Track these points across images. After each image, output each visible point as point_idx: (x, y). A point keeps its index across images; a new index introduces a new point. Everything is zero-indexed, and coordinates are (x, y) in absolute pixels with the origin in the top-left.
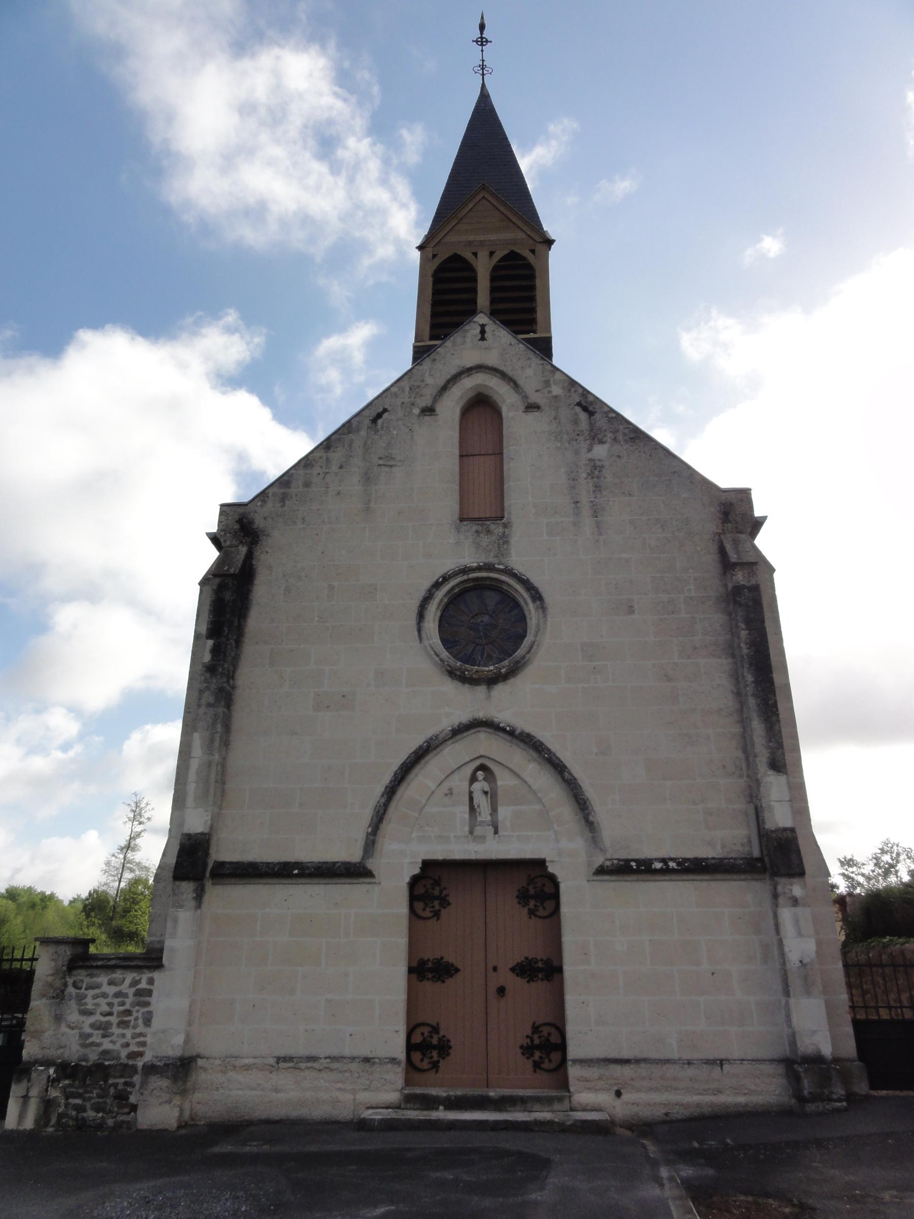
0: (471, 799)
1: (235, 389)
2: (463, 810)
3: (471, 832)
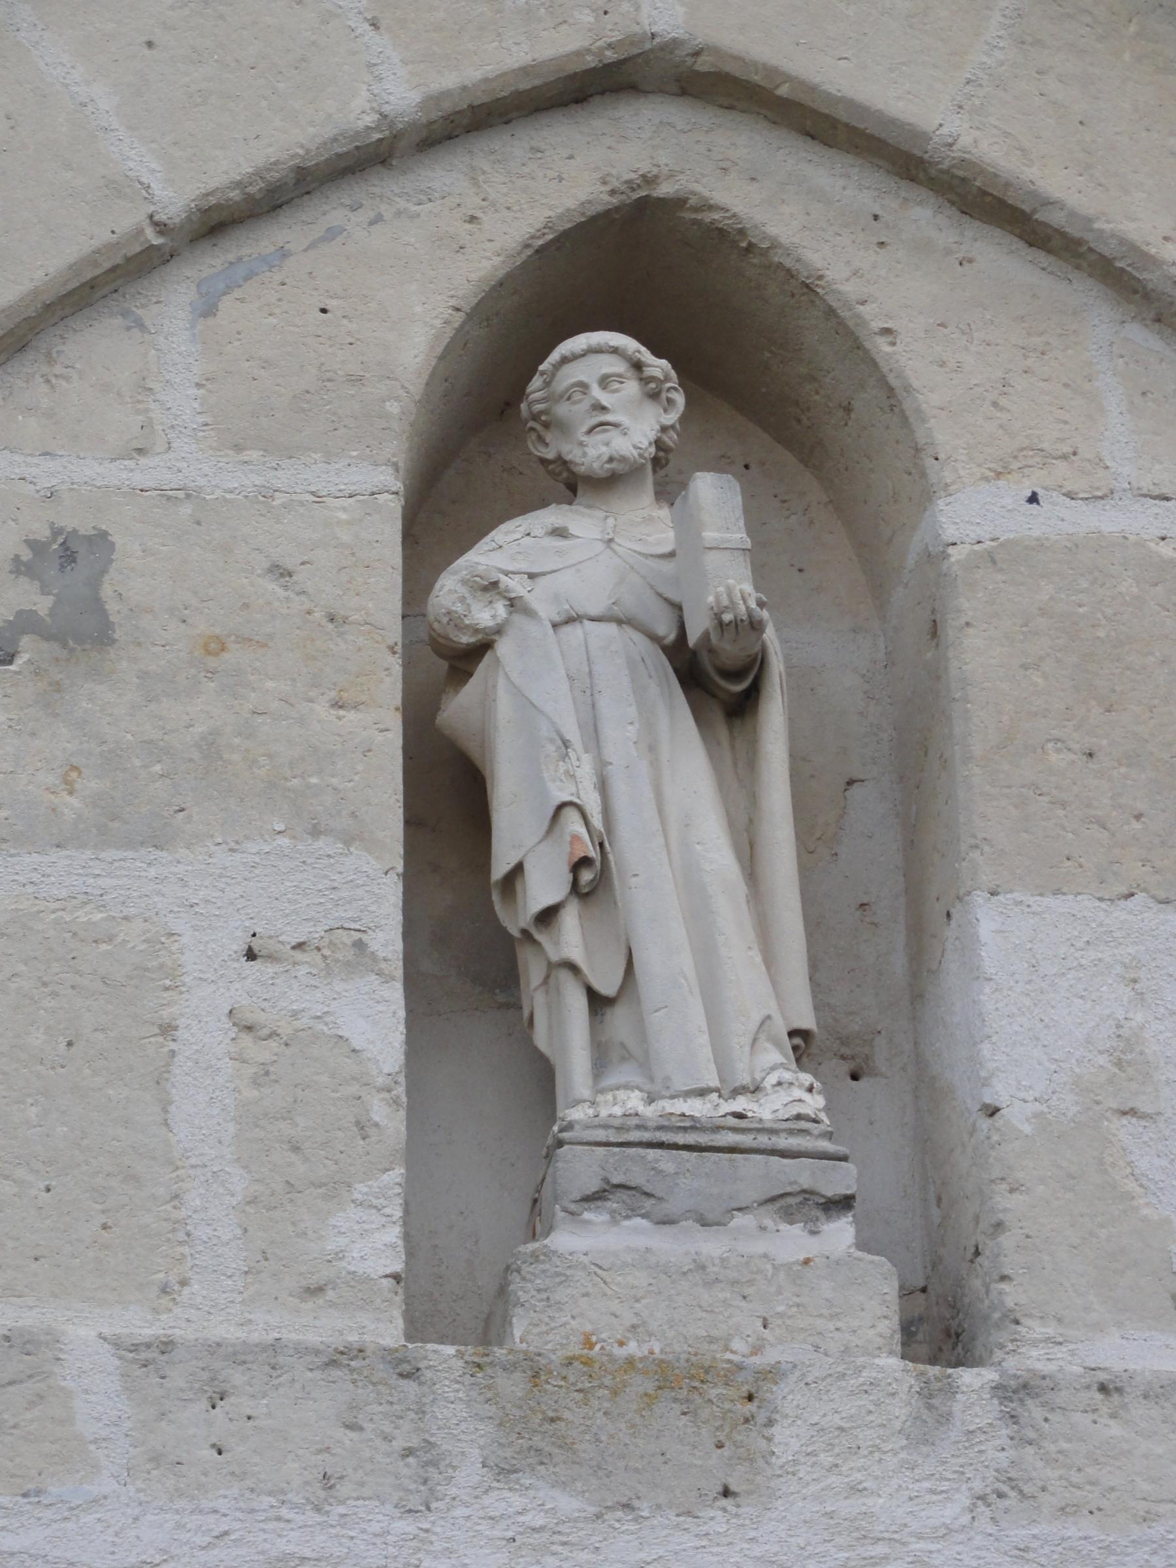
0: (448, 795)
1: (892, 397)
2: (285, 923)
3: (458, 1298)
